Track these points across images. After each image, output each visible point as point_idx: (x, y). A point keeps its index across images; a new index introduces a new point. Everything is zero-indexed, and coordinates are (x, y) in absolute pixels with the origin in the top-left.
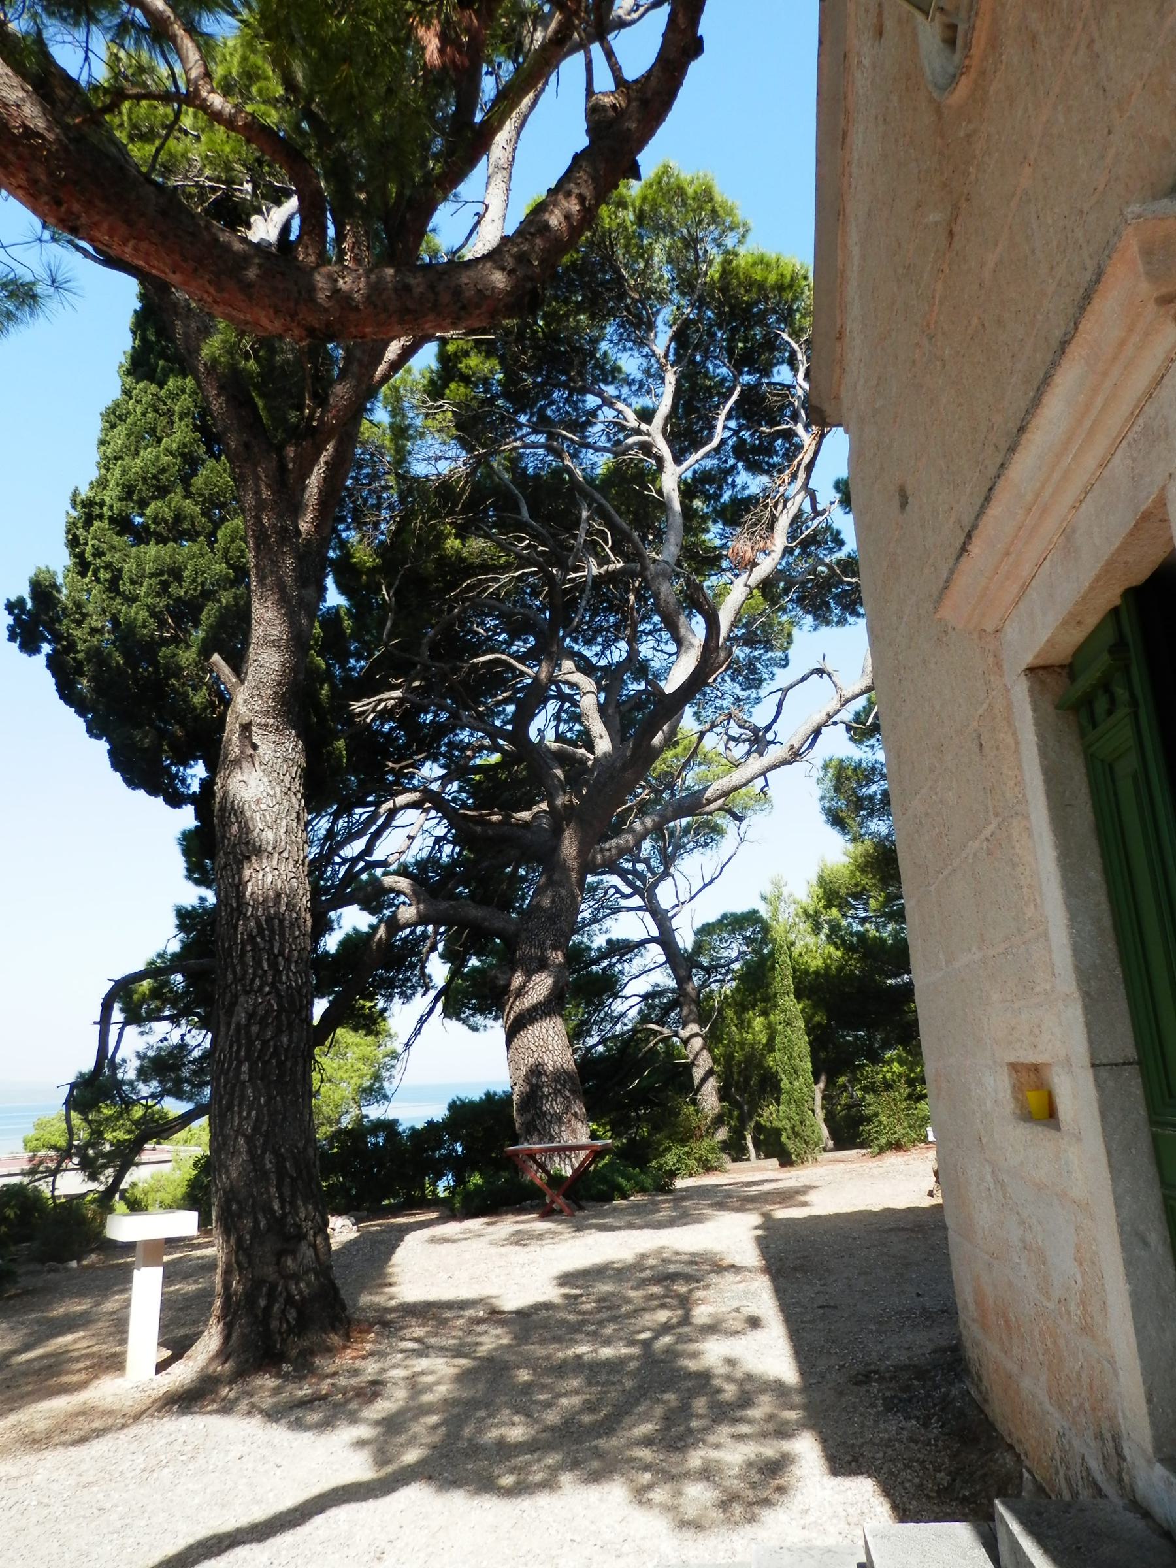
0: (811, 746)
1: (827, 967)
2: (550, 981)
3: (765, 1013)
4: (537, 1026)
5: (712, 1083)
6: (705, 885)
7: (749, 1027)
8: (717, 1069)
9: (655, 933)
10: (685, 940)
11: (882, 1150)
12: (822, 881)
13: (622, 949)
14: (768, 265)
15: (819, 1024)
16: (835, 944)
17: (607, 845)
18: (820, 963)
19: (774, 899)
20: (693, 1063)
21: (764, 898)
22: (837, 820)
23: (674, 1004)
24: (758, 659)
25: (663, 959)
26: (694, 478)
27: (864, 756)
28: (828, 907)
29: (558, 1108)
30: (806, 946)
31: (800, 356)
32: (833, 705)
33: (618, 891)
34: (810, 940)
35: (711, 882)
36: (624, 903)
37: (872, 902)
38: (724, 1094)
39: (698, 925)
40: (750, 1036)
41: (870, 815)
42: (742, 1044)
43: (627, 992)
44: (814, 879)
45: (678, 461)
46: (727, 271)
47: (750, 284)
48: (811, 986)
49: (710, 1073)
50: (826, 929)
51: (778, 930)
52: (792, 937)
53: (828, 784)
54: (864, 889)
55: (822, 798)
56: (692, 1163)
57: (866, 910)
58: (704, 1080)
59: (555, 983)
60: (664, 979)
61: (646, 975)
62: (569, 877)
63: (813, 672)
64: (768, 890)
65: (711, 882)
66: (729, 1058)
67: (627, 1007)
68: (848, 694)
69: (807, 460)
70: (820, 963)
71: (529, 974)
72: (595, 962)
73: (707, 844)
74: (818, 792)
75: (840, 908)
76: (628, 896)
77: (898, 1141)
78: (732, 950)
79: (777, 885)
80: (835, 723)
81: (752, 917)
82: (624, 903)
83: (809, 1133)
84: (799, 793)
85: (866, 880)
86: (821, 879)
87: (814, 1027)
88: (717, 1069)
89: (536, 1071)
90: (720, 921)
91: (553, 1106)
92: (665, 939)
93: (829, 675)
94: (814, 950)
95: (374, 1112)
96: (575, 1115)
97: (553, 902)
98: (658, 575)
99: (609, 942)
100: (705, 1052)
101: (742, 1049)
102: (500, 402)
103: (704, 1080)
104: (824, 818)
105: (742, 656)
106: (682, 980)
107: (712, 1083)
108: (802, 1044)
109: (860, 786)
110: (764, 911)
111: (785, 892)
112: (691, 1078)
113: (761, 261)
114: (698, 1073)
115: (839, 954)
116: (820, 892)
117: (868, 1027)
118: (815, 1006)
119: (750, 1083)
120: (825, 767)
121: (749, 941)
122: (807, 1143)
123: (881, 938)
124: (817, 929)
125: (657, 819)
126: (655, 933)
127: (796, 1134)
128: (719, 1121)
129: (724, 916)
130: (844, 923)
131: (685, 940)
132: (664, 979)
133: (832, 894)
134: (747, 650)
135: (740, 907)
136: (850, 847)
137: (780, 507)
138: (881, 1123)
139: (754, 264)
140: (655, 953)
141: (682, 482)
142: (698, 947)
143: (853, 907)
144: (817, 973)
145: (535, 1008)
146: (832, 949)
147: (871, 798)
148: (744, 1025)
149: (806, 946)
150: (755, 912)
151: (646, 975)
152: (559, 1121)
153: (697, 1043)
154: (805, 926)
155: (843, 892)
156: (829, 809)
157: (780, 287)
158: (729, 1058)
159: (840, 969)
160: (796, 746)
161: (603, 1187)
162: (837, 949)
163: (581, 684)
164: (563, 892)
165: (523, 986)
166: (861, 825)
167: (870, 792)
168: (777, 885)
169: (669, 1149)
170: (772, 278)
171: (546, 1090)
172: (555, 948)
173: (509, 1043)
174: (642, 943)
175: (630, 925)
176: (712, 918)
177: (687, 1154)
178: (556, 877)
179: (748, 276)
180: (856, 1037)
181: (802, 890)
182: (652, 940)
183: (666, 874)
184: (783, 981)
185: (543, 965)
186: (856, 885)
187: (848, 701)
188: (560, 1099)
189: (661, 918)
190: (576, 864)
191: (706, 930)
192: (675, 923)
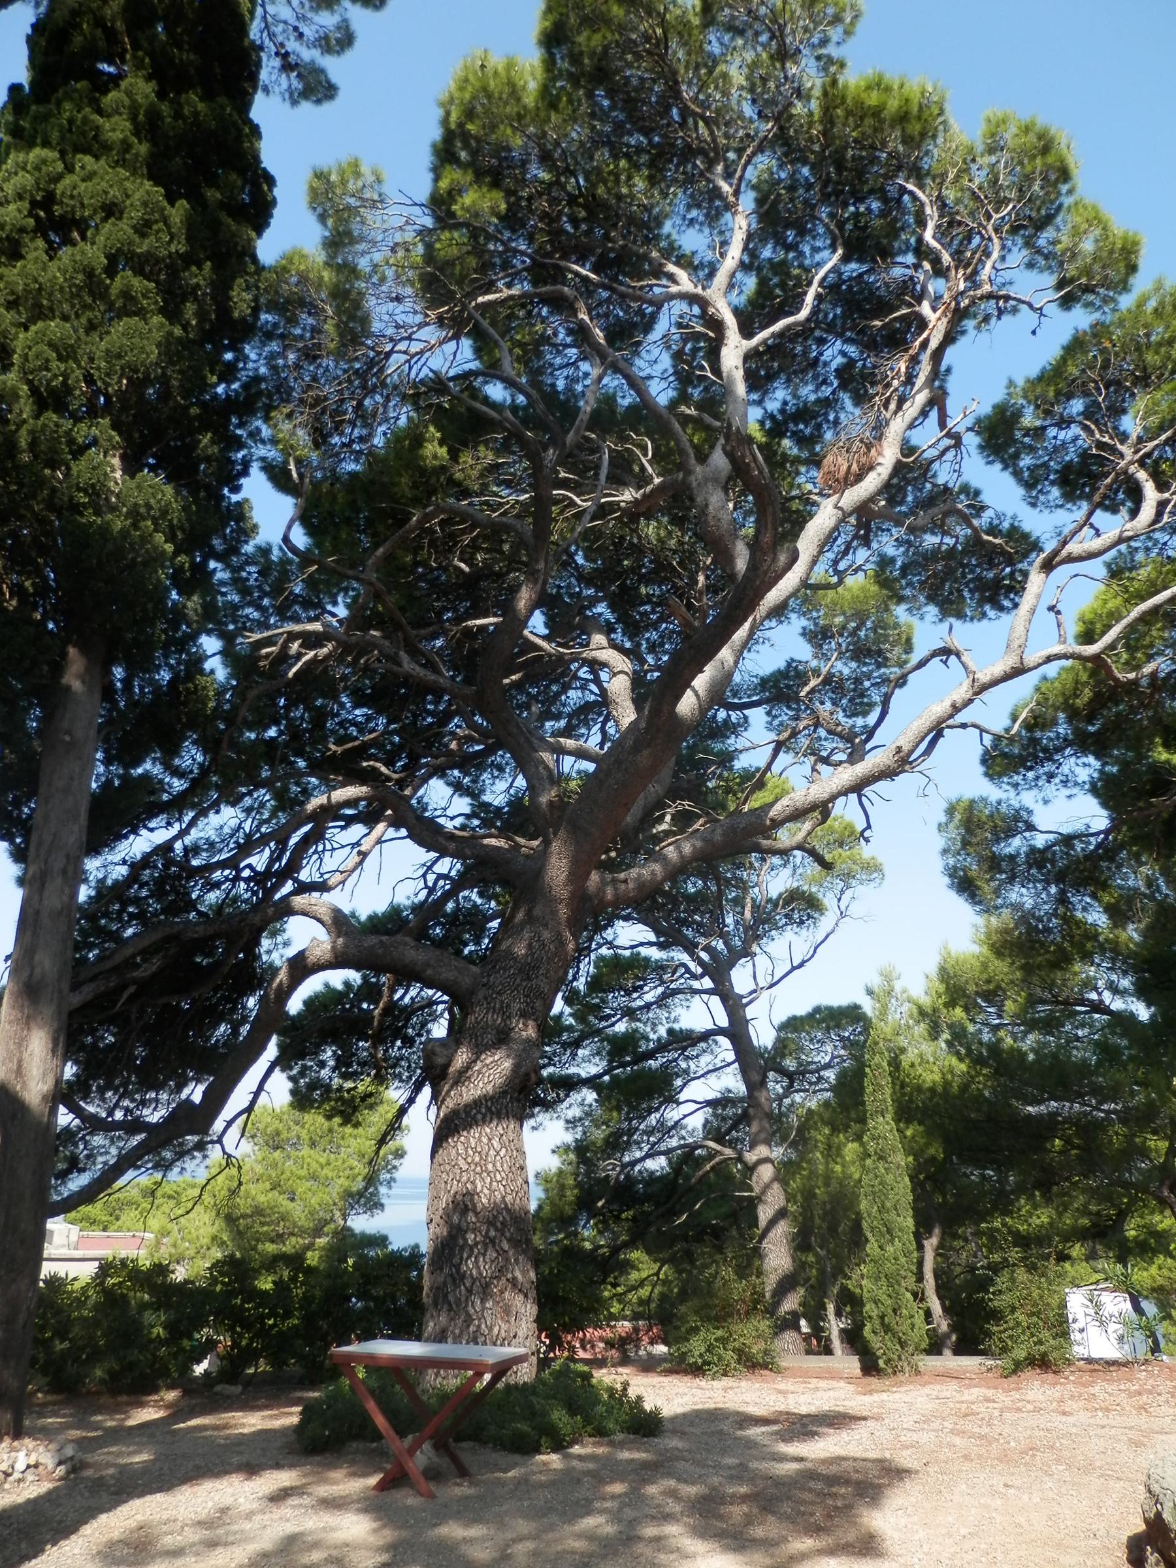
0: (928, 751)
1: (947, 1084)
2: (507, 1064)
3: (858, 1138)
4: (475, 1132)
5: (782, 1229)
6: (794, 969)
7: (839, 1154)
8: (792, 1208)
9: (723, 1021)
10: (763, 1035)
11: (1018, 1367)
12: (944, 974)
13: (684, 1040)
14: (888, 89)
15: (933, 1159)
16: (958, 1053)
17: (622, 876)
18: (937, 1077)
19: (883, 995)
20: (759, 1199)
21: (870, 992)
22: (965, 885)
23: (744, 1118)
24: (868, 676)
25: (731, 1056)
26: (782, 411)
27: (1004, 796)
28: (951, 1004)
29: (486, 1269)
30: (921, 1056)
31: (928, 210)
32: (962, 692)
33: (688, 970)
34: (927, 1048)
35: (801, 965)
36: (696, 985)
37: (1009, 1006)
38: (801, 1244)
39: (780, 1017)
40: (838, 1168)
41: (1011, 879)
42: (828, 1178)
43: (682, 1097)
44: (933, 970)
45: (747, 332)
46: (832, 96)
47: (861, 112)
48: (912, 1105)
49: (781, 1214)
50: (946, 1036)
51: (883, 1029)
52: (903, 1041)
53: (955, 832)
54: (998, 987)
55: (945, 852)
56: (730, 1356)
57: (1000, 1017)
58: (772, 1223)
59: (516, 1068)
60: (732, 1082)
61: (713, 1078)
62: (554, 913)
63: (934, 654)
64: (876, 982)
65: (801, 965)
66: (809, 1195)
67: (689, 1113)
68: (983, 677)
69: (934, 344)
70: (937, 1077)
71: (479, 1050)
72: (651, 1054)
73: (802, 922)
74: (940, 842)
75: (966, 1009)
76: (694, 976)
77: (1044, 1355)
78: (825, 1053)
79: (888, 977)
80: (964, 726)
81: (852, 1014)
82: (696, 985)
83: (905, 1327)
84: (907, 830)
85: (1001, 968)
86: (943, 970)
87: (927, 1161)
88: (792, 1208)
89: (463, 1205)
90: (811, 1016)
91: (477, 1266)
92: (737, 1032)
93: (958, 655)
94: (932, 1061)
95: (361, 1223)
96: (514, 1282)
97: (530, 946)
98: (706, 480)
99: (670, 1032)
100: (776, 1186)
101: (827, 1184)
102: (650, 530)
103: (772, 1223)
104: (947, 880)
105: (846, 671)
106: (755, 1084)
107: (782, 1229)
108: (902, 1190)
109: (998, 840)
110: (868, 1007)
111: (898, 986)
112: (756, 1219)
113: (878, 84)
114: (764, 1214)
115: (963, 1067)
116: (942, 988)
117: (999, 1166)
118: (929, 1133)
119: (832, 1232)
120: (951, 811)
121: (846, 1043)
122: (903, 1344)
123: (1019, 1050)
124: (934, 1033)
125: (699, 844)
126: (723, 1021)
127: (887, 1329)
128: (786, 1285)
129: (817, 1010)
130: (971, 1028)
131: (763, 1035)
132: (732, 1082)
133: (955, 988)
134: (854, 665)
135: (838, 999)
136: (980, 921)
137: (893, 406)
138: (1018, 1324)
139: (869, 88)
140: (725, 1049)
141: (747, 357)
142: (781, 1047)
143: (982, 1010)
144: (932, 1090)
145: (476, 1103)
146: (954, 1061)
147: (1012, 858)
148: (833, 1151)
149: (921, 1056)
150: (857, 1007)
151: (713, 1078)
152: (485, 1291)
153: (766, 1172)
154: (921, 1029)
155: (972, 988)
156: (955, 868)
157: (903, 118)
158: (809, 1195)
159: (964, 1087)
160: (906, 748)
161: (523, 1427)
162: (961, 1060)
163: (611, 662)
164: (546, 935)
165: (468, 1067)
166: (997, 892)
167: (1009, 850)
168: (888, 977)
169: (695, 1330)
170: (893, 104)
171: (471, 1237)
172: (524, 1015)
173: (432, 1157)
174: (706, 1036)
175: (699, 1013)
176: (802, 1010)
177: (723, 1341)
178: (537, 911)
179: (859, 104)
180: (983, 1176)
181: (918, 983)
182: (720, 1031)
183: (747, 953)
184: (880, 1094)
185: (502, 1038)
186: (988, 981)
187: (985, 688)
188: (491, 1254)
189: (734, 1005)
190: (565, 894)
191: (792, 1024)
192: (750, 1012)
